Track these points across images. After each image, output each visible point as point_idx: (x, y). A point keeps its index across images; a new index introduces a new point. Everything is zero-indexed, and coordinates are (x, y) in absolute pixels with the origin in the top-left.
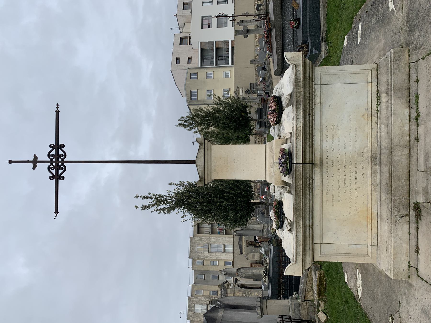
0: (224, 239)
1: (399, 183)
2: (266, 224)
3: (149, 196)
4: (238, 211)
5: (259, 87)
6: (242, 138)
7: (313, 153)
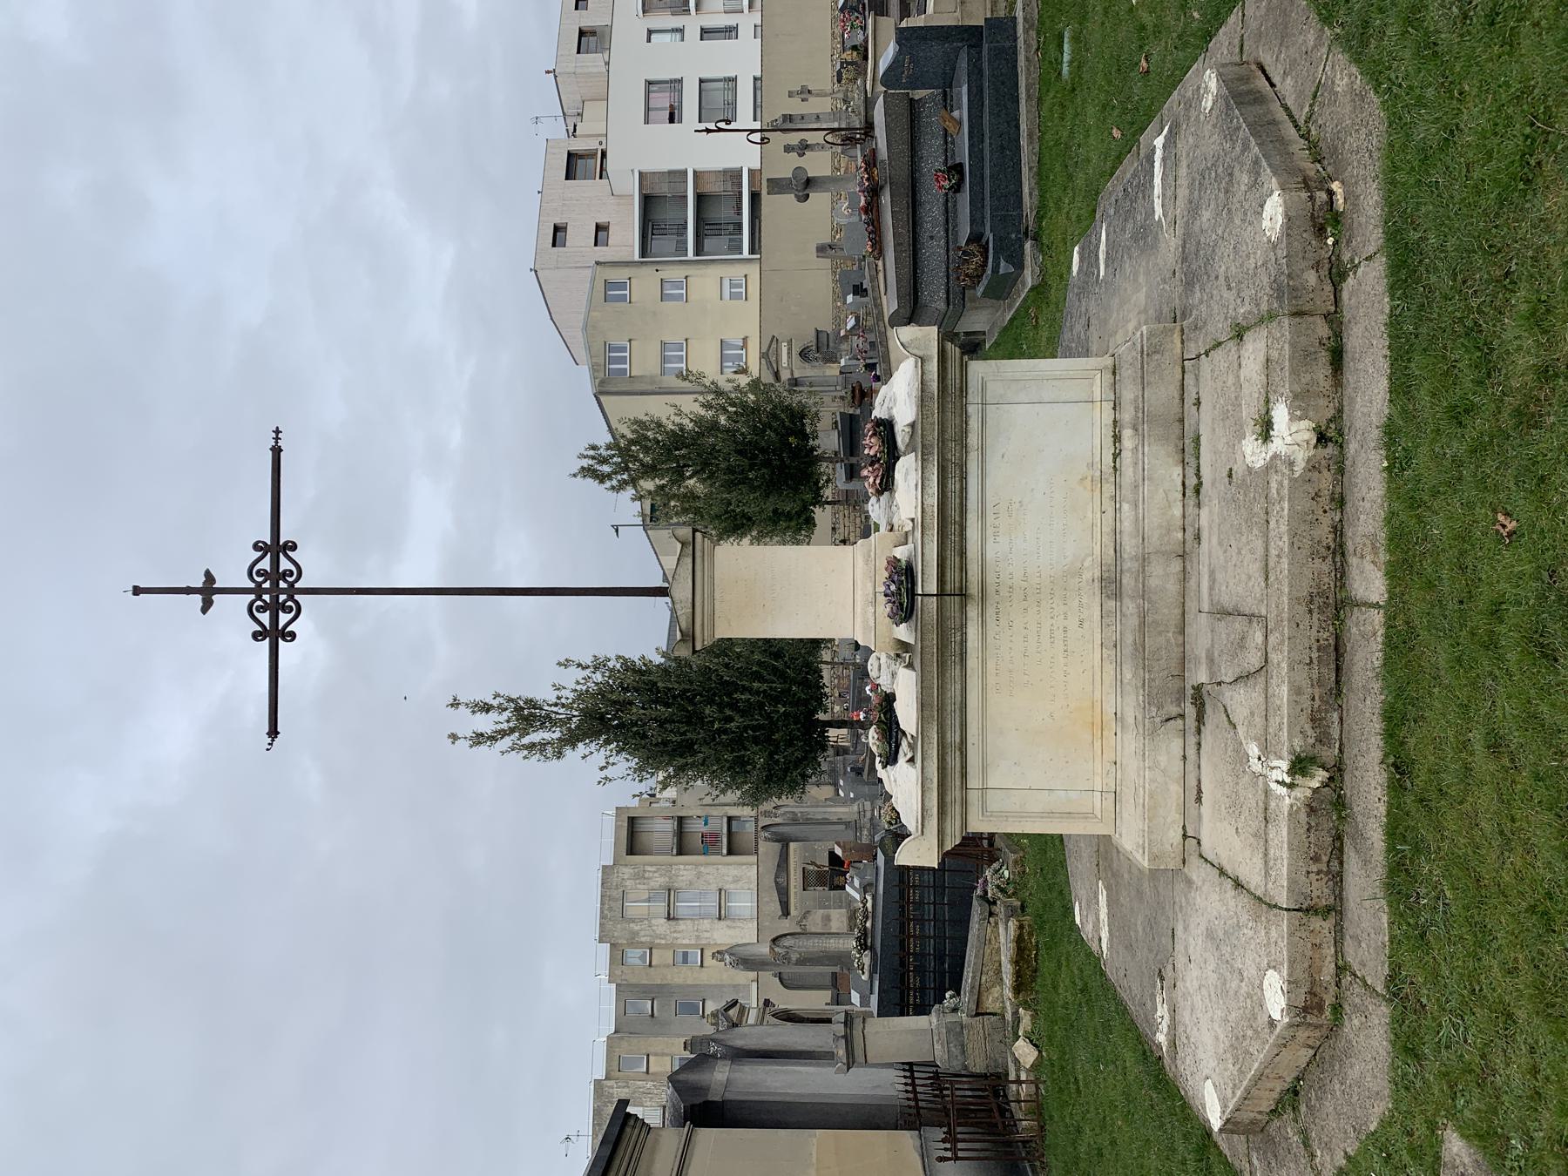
0: (723, 870)
1: (1162, 640)
2: (868, 804)
3: (495, 703)
4: (778, 747)
5: (844, 346)
6: (789, 517)
7: (963, 568)
